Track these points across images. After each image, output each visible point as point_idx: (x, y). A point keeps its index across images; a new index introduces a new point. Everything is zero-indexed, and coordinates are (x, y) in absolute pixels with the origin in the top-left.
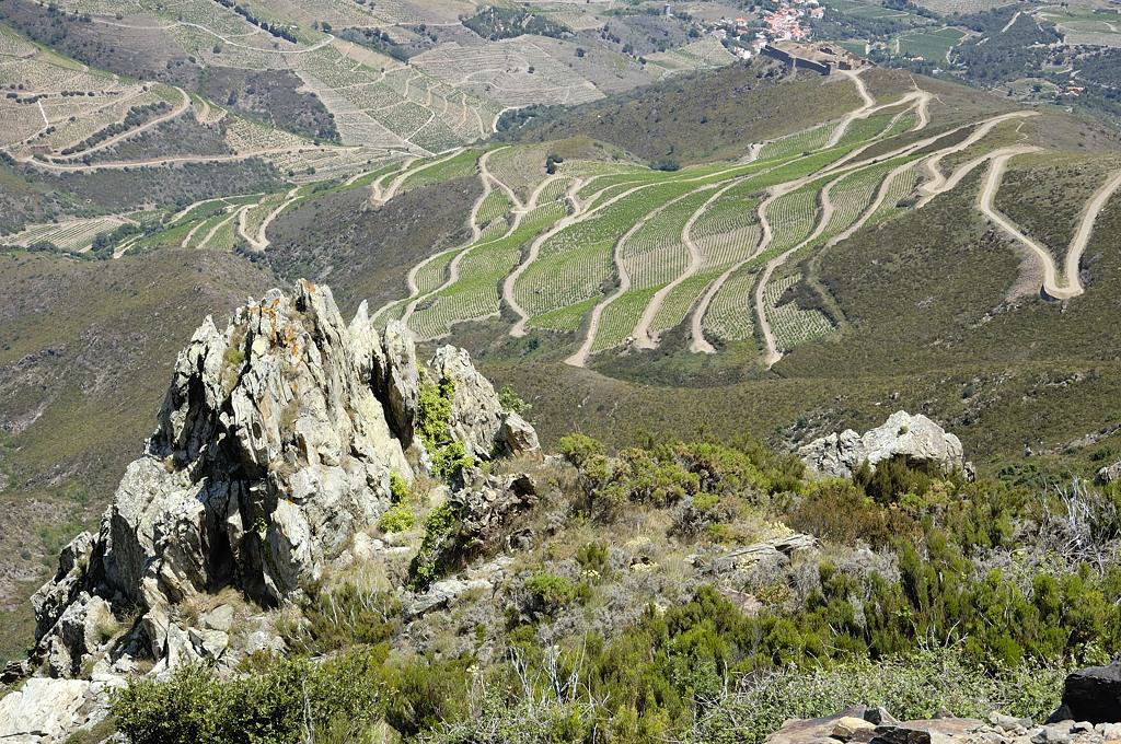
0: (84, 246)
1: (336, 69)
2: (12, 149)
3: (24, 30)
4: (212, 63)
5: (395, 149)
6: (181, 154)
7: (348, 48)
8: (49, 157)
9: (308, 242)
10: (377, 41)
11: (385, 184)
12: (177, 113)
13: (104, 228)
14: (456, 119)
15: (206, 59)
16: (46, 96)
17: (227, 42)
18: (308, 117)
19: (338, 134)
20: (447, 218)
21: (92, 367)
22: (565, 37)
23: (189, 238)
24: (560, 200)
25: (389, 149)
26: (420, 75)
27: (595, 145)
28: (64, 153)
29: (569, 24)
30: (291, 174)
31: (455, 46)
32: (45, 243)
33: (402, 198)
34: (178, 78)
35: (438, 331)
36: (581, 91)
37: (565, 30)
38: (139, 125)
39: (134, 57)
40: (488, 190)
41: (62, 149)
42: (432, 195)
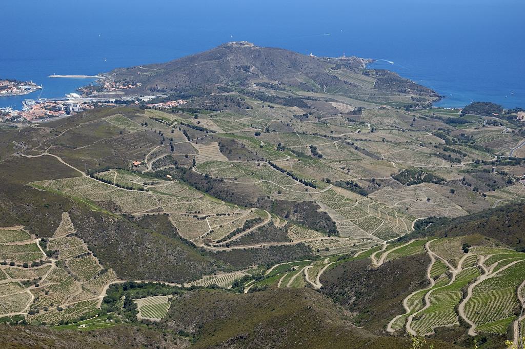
0: (229, 286)
1: (335, 200)
2: (195, 241)
3: (194, 186)
4: (277, 198)
5: (366, 238)
6: (269, 242)
7: (339, 190)
8: (211, 244)
9: (342, 285)
10: (352, 187)
11: (378, 256)
12: (266, 222)
13: (236, 278)
14: (394, 224)
15: (275, 196)
16: (210, 216)
17: (284, 189)
18: (323, 223)
19: (338, 232)
20: (414, 274)
21: (261, 345)
22: (444, 184)
23: (280, 282)
24: (475, 266)
25: (363, 239)
26: (374, 203)
27: (486, 239)
28: (218, 242)
29: (445, 177)
30: (318, 251)
31: (389, 188)
32: (214, 285)
33: (387, 264)
34: (263, 206)
35: (428, 331)
36: (454, 210)
37: (443, 180)
38: (249, 228)
39: (243, 197)
40: (433, 261)
41: (217, 240)
42: (404, 262)
